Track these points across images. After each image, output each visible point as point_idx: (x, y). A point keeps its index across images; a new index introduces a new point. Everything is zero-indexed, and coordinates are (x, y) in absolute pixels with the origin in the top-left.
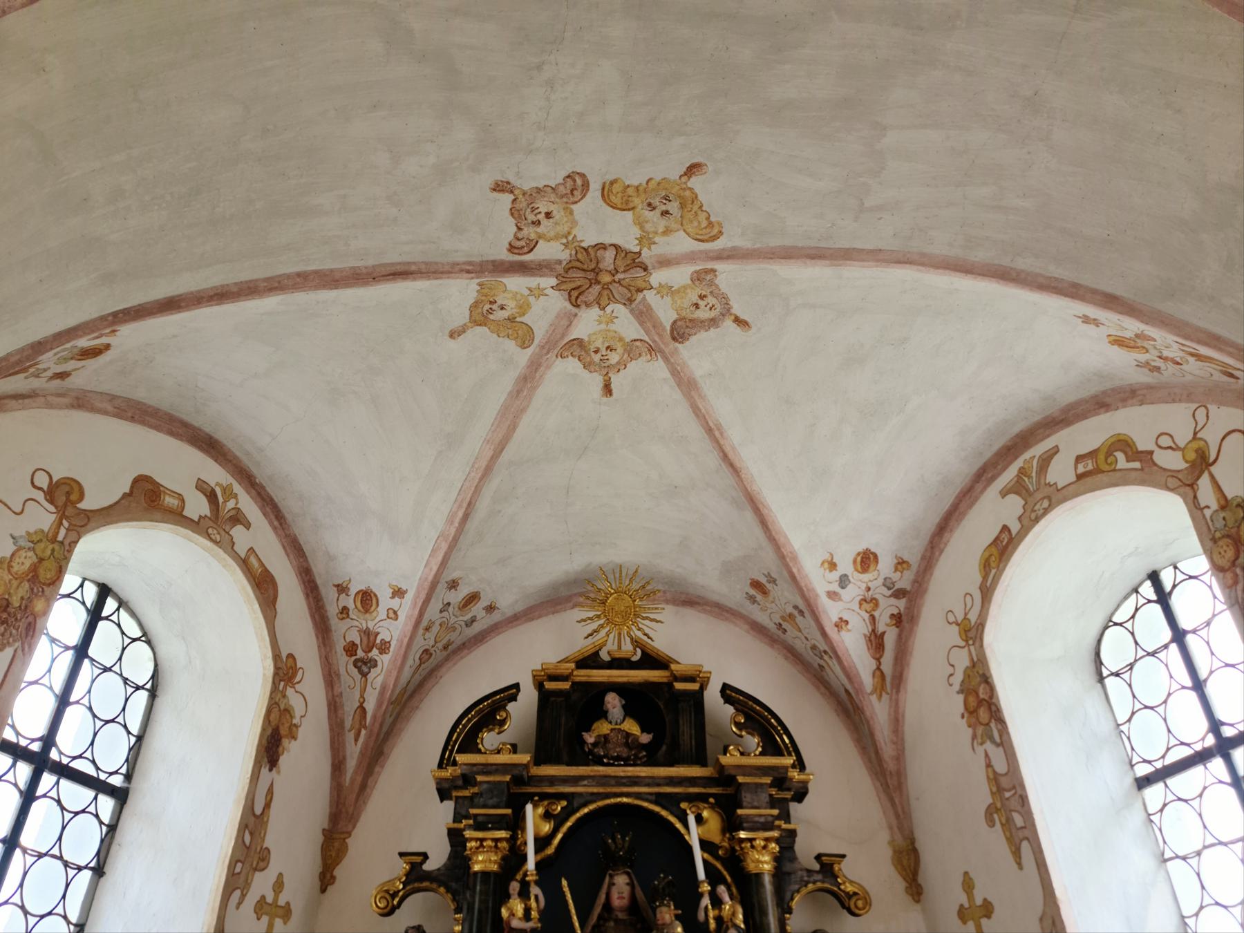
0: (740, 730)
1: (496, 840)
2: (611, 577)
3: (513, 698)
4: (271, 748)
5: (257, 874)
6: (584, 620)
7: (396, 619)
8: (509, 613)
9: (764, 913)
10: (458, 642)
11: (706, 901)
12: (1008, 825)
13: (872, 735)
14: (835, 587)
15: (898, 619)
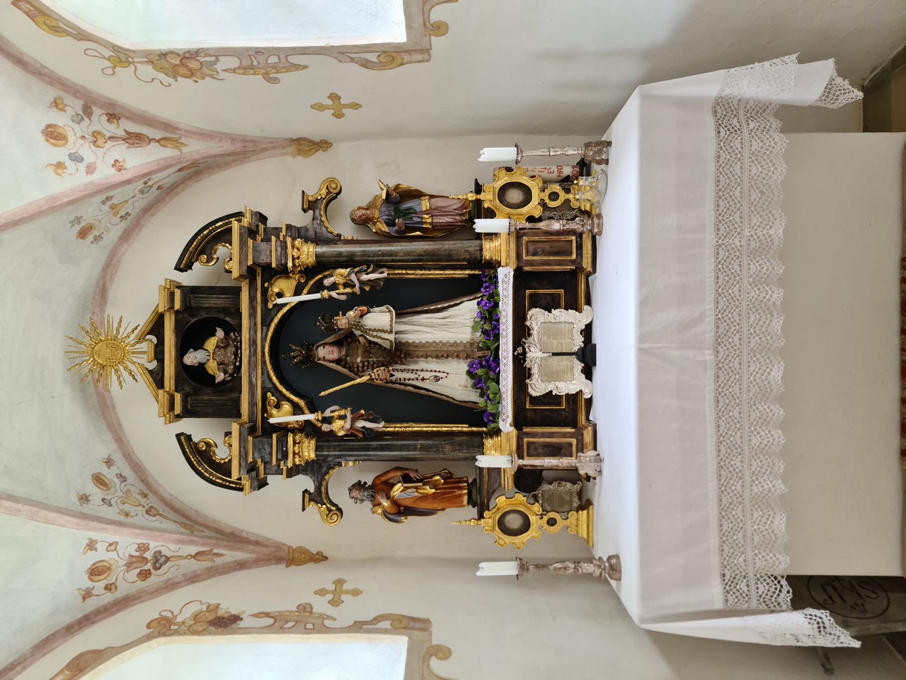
0: (212, 259)
1: (295, 443)
2: (78, 361)
3: (189, 438)
4: (224, 623)
5: (314, 610)
7: (117, 543)
8: (114, 446)
9: (340, 254)
11: (334, 294)
12: (277, 68)
13: (215, 156)
14: (82, 166)
15: (112, 117)
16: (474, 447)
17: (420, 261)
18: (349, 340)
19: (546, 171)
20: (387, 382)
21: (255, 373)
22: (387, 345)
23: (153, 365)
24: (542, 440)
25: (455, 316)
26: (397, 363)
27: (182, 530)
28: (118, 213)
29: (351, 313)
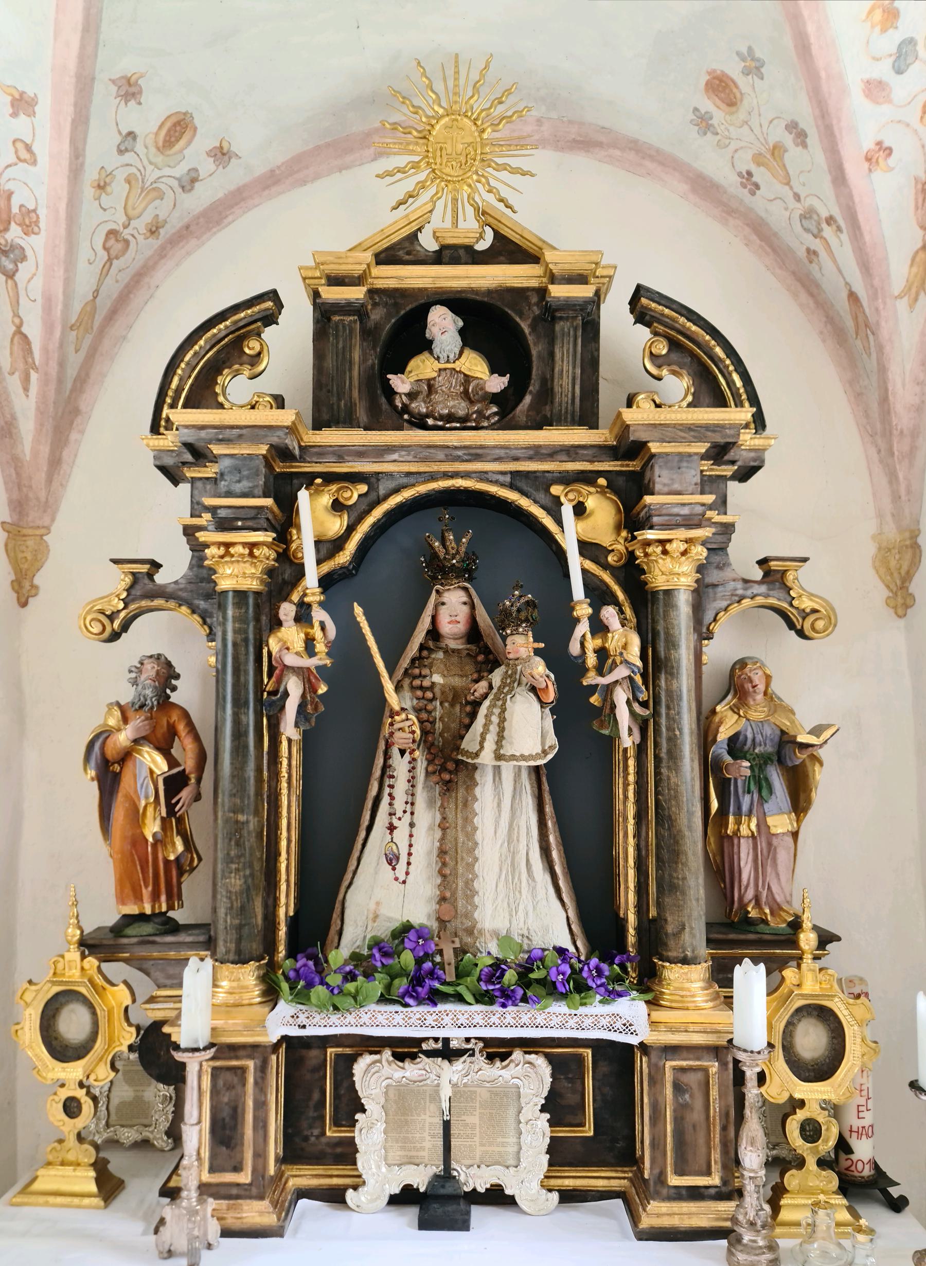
0: (659, 367)
1: (252, 546)
2: (439, 87)
3: (270, 319)
6: (390, 174)
7: (34, 163)
8: (260, 169)
9: (672, 644)
10: (175, 224)
11: (583, 628)
13: (882, 370)
14: (883, 70)
16: (239, 941)
17: (658, 814)
18: (481, 658)
19: (862, 1101)
20: (388, 746)
21: (405, 458)
22: (469, 743)
23: (428, 243)
24: (250, 1103)
25: (533, 890)
26: (430, 762)
27: (77, 307)
28: (759, 164)
29: (539, 668)
